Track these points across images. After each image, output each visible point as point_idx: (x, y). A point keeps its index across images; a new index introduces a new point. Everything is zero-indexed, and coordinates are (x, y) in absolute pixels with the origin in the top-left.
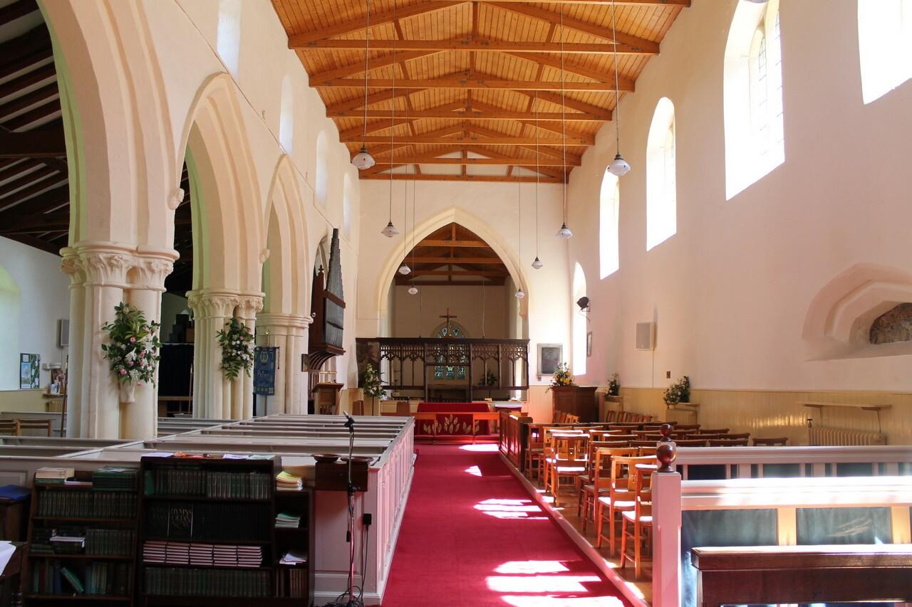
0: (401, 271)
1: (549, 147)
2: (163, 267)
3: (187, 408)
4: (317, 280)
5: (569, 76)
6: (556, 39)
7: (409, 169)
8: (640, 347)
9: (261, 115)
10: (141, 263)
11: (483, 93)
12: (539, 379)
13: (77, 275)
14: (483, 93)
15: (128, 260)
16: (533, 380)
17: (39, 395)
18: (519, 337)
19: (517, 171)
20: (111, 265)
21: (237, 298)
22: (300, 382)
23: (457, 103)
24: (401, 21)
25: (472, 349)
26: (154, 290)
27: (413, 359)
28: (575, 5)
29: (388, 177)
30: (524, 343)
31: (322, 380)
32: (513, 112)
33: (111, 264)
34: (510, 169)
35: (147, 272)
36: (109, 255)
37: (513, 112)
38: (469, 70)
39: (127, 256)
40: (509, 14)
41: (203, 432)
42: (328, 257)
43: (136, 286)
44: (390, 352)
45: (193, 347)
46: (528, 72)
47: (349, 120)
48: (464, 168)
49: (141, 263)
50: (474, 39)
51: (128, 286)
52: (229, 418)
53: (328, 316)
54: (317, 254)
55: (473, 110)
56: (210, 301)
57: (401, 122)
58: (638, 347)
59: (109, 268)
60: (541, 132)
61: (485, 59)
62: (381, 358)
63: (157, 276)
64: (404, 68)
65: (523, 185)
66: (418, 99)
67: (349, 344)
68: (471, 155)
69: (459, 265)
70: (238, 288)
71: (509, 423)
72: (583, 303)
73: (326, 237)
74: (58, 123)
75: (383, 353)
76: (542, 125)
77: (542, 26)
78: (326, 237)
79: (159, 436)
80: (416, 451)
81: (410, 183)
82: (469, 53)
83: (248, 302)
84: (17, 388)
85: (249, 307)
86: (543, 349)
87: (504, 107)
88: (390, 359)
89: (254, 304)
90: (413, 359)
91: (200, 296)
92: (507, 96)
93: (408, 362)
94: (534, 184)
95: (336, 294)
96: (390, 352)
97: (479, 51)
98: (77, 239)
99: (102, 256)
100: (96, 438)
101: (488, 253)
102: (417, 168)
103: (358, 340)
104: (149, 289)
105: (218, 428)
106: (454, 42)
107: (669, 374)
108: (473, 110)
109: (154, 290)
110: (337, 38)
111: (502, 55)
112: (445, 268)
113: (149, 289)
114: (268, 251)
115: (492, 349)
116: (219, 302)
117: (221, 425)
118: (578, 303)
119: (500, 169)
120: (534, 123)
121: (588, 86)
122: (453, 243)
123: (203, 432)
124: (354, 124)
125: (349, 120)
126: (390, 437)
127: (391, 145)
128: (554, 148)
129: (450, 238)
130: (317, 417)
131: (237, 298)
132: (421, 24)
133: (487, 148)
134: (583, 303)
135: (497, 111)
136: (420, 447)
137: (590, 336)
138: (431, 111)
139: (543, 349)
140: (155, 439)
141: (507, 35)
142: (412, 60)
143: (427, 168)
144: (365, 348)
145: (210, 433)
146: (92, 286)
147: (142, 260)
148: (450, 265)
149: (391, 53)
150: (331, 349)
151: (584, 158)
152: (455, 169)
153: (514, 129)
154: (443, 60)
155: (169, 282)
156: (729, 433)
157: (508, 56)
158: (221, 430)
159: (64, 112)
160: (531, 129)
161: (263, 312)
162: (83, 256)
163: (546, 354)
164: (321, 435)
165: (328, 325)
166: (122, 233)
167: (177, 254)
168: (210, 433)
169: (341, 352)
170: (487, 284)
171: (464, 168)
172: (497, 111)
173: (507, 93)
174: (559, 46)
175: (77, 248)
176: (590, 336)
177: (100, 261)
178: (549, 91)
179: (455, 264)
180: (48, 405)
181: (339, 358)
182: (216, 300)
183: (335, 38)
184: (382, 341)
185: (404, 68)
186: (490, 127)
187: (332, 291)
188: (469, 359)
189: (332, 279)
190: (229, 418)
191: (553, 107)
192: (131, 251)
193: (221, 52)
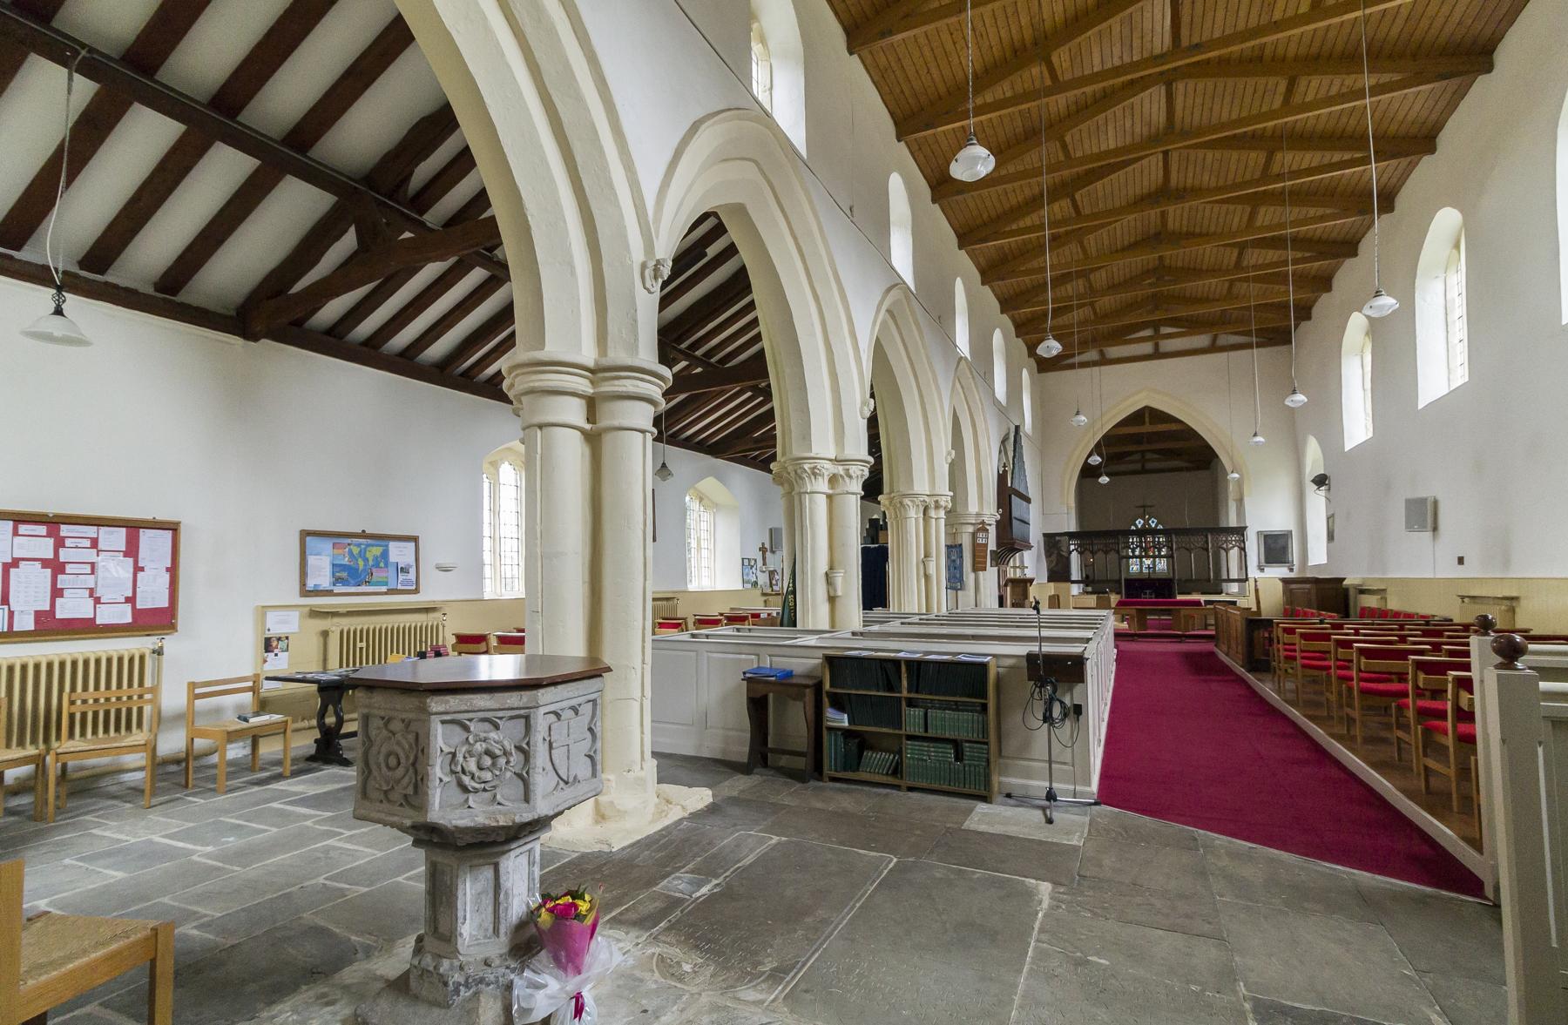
0: (1090, 461)
1: (1266, 304)
2: (859, 473)
3: (883, 602)
4: (1002, 478)
5: (1292, 213)
6: (1236, 252)
7: (1092, 355)
8: (1412, 527)
9: (848, 212)
10: (840, 470)
11: (1175, 255)
12: (1262, 570)
13: (786, 485)
14: (1175, 255)
15: (829, 468)
16: (1253, 573)
17: (758, 592)
18: (1233, 522)
19: (1224, 339)
20: (815, 474)
21: (926, 499)
22: (990, 577)
23: (1147, 273)
24: (1078, 196)
25: (1174, 539)
26: (853, 494)
27: (1106, 553)
28: (1301, 120)
29: (1072, 367)
30: (1240, 531)
31: (1011, 574)
32: (1214, 271)
33: (815, 473)
34: (1215, 338)
35: (847, 479)
36: (812, 466)
37: (1214, 271)
38: (1160, 233)
39: (827, 465)
40: (1210, 154)
41: (902, 623)
42: (1011, 454)
43: (838, 491)
44: (1079, 545)
45: (886, 549)
46: (1236, 220)
47: (1012, 283)
48: (1157, 346)
49: (840, 470)
50: (1164, 194)
51: (830, 492)
52: (924, 612)
53: (1015, 514)
54: (1000, 452)
55: (1166, 278)
56: (901, 503)
57: (1083, 305)
58: (1410, 526)
59: (813, 477)
60: (1254, 288)
61: (1177, 216)
62: (1071, 552)
63: (855, 481)
64: (1083, 247)
65: (1233, 354)
66: (1100, 279)
67: (1035, 536)
68: (1165, 330)
69: (1154, 451)
70: (927, 488)
71: (1228, 618)
72: (1321, 481)
73: (1008, 434)
74: (762, 352)
75: (1072, 547)
76: (1257, 279)
77: (1256, 158)
78: (1008, 434)
79: (864, 626)
80: (1116, 646)
81: (1096, 369)
82: (1159, 214)
83: (937, 502)
84: (741, 588)
85: (937, 506)
86: (1266, 536)
87: (1204, 268)
88: (1081, 553)
89: (943, 503)
90: (1106, 553)
91: (891, 500)
92: (1207, 252)
93: (1100, 555)
94: (1249, 351)
95: (1022, 490)
96: (1079, 545)
97: (1171, 209)
98: (784, 454)
99: (806, 467)
100: (810, 628)
101: (1190, 434)
102: (1102, 353)
103: (1045, 535)
104: (848, 493)
105: (916, 619)
106: (1142, 202)
107: (1461, 561)
108: (1166, 278)
109: (853, 494)
110: (1007, 229)
111: (1200, 208)
112: (1137, 457)
113: (848, 493)
114: (953, 452)
115: (1197, 541)
116: (909, 503)
117: (918, 617)
118: (1313, 481)
119: (1202, 340)
120: (1246, 279)
121: (1322, 218)
122: (1147, 428)
123: (902, 623)
124: (1029, 316)
125: (1012, 283)
126: (1092, 628)
127: (1072, 305)
128: (1272, 305)
129: (1143, 423)
130: (1008, 610)
131: (926, 499)
132: (1100, 194)
133: (1269, 133)
134: (1321, 481)
135: (1194, 272)
136: (1118, 643)
137: (1331, 521)
138: (1113, 287)
139: (1266, 536)
140: (861, 629)
141: (1207, 179)
142: (1091, 237)
143: (1114, 351)
144: (1053, 542)
145: (909, 624)
146: (800, 494)
147: (841, 468)
148: (1143, 452)
149: (1067, 233)
150: (1019, 544)
151: (1315, 311)
152: (1147, 348)
153: (1218, 291)
154: (1128, 226)
155: (866, 486)
156: (1532, 633)
157: (1208, 207)
158: (918, 621)
159: (765, 343)
160: (1242, 288)
161: (950, 512)
162: (790, 469)
163: (1270, 541)
164: (1017, 627)
165: (1014, 521)
166: (823, 445)
167: (872, 460)
168: (909, 624)
169: (1029, 547)
170: (1188, 469)
171: (1157, 346)
172: (1194, 272)
173: (1208, 252)
174: (1280, 177)
175: (785, 462)
176: (1331, 521)
177: (806, 471)
178: (1265, 238)
179: (1149, 451)
180: (765, 601)
181: (1026, 554)
182: (907, 501)
183: (932, 7)
184: (1071, 535)
185: (1083, 247)
186: (1188, 295)
187: (1016, 486)
188: (1172, 549)
189: (1016, 475)
190: (924, 612)
191: (1271, 255)
192: (831, 460)
193: (895, 263)
